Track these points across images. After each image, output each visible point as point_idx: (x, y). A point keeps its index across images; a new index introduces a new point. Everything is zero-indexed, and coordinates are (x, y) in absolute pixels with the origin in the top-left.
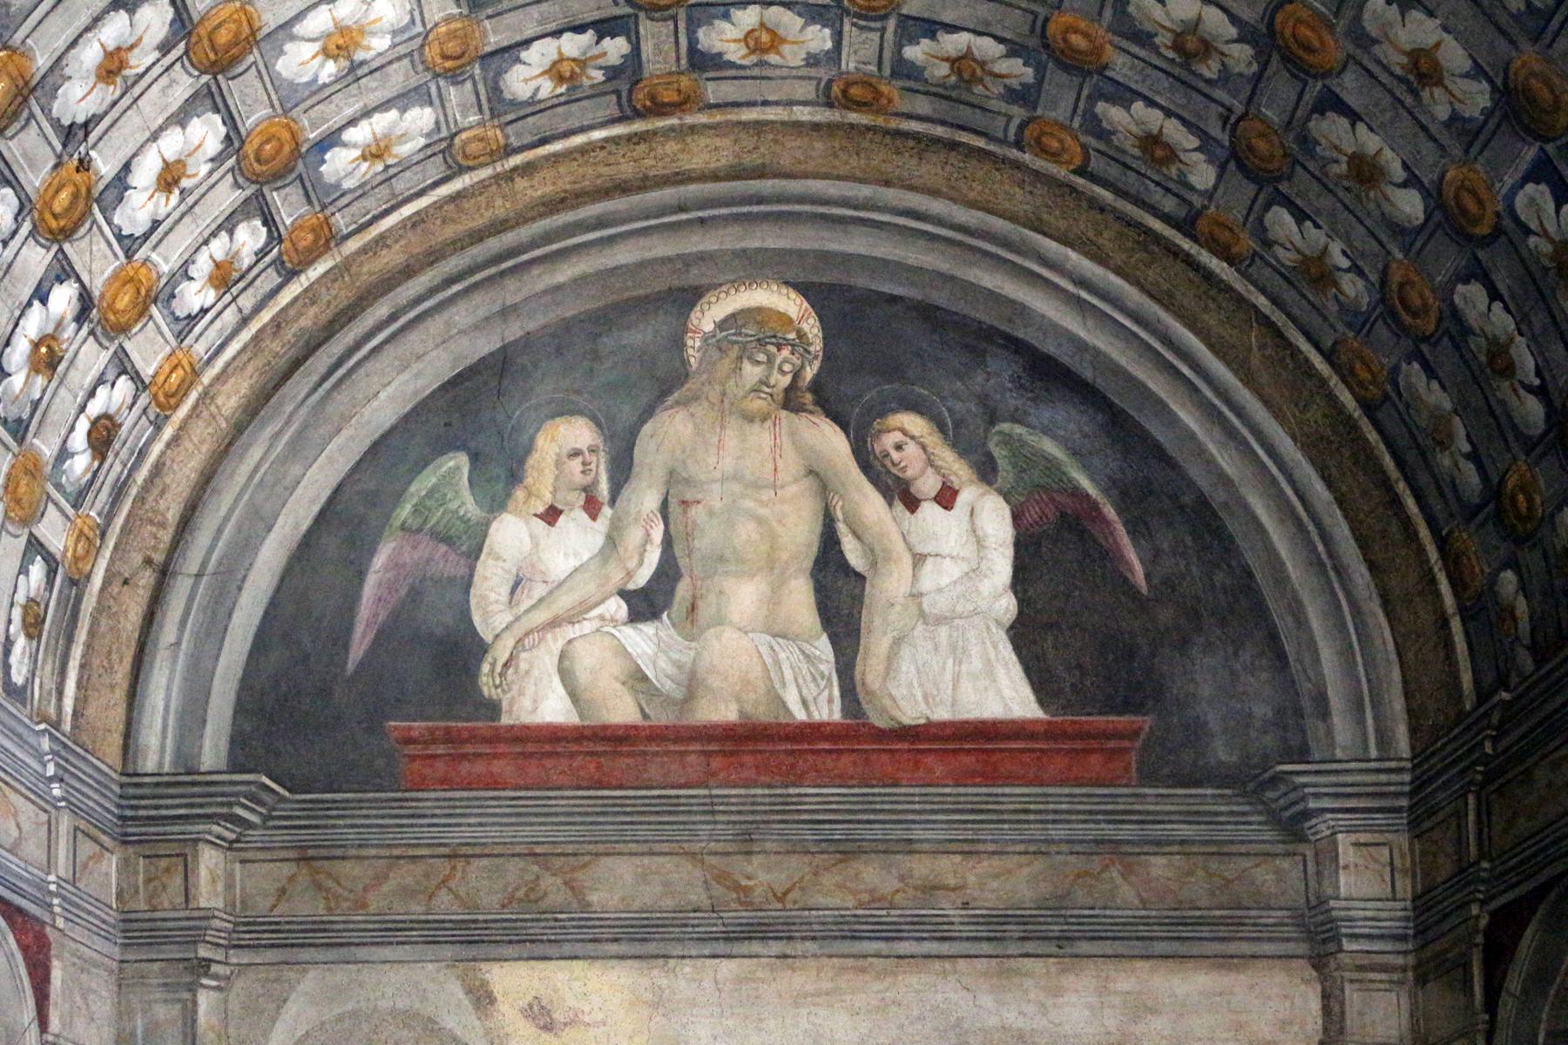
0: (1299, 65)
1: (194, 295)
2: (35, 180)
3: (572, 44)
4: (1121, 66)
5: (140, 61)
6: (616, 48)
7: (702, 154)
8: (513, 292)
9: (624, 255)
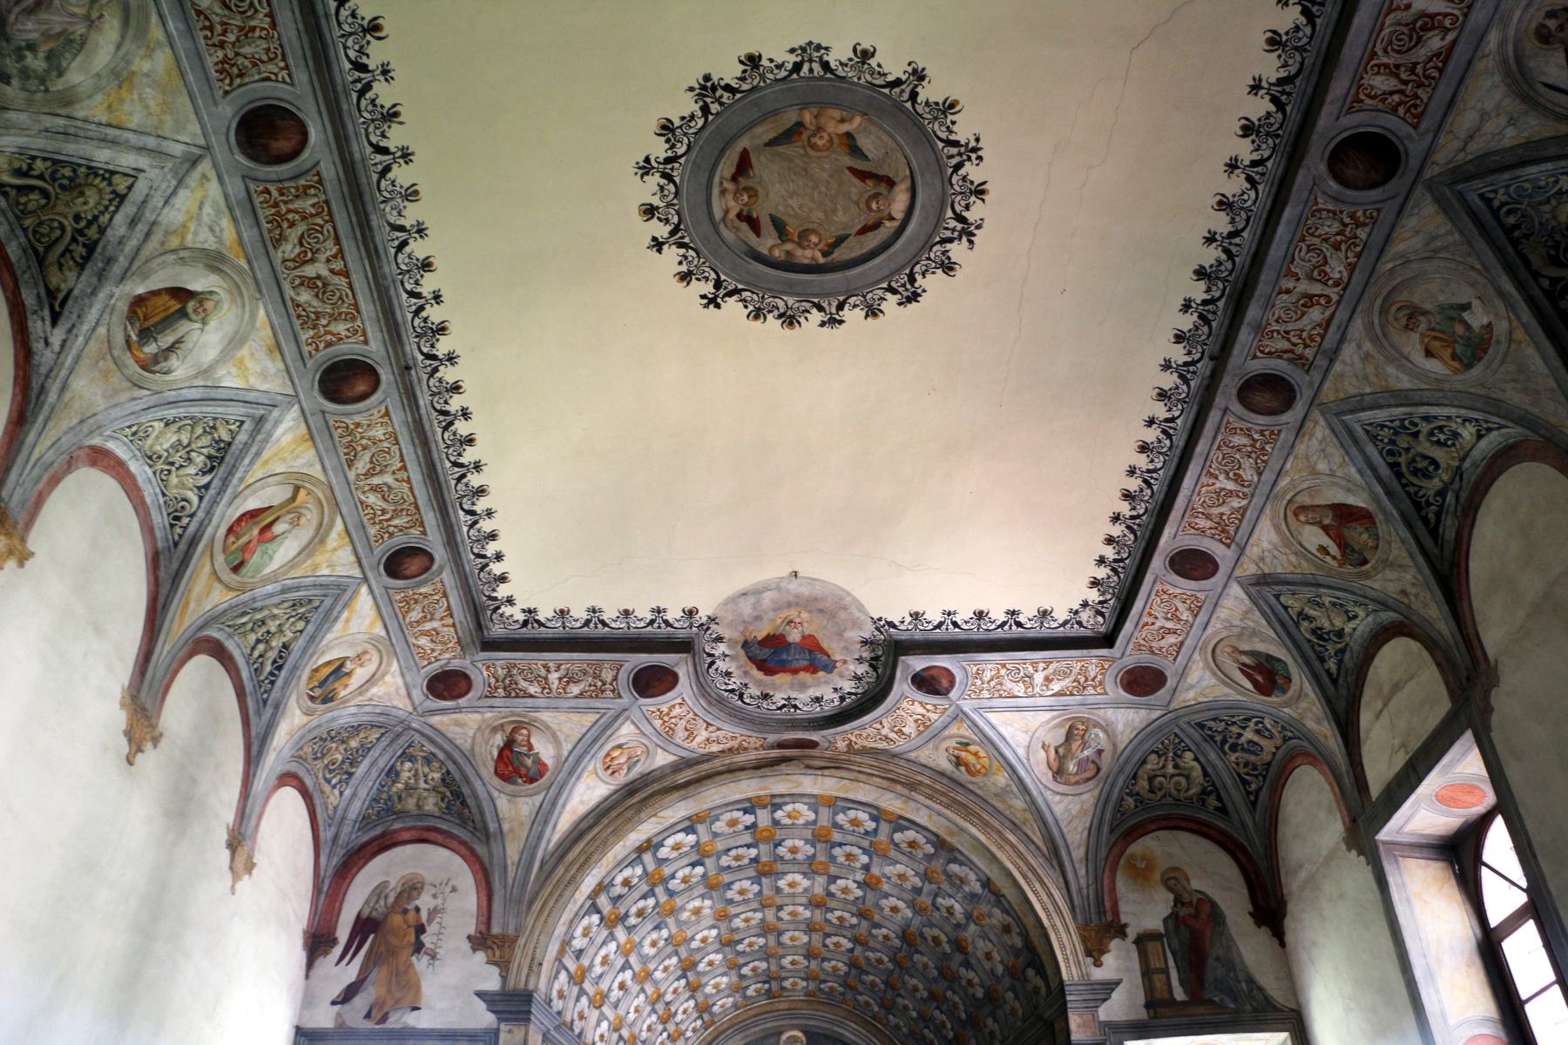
1: (689, 1034)
2: (661, 1012)
3: (759, 985)
4: (860, 988)
5: (680, 990)
6: (767, 986)
7: (782, 1006)
8: (748, 1032)
9: (768, 1025)
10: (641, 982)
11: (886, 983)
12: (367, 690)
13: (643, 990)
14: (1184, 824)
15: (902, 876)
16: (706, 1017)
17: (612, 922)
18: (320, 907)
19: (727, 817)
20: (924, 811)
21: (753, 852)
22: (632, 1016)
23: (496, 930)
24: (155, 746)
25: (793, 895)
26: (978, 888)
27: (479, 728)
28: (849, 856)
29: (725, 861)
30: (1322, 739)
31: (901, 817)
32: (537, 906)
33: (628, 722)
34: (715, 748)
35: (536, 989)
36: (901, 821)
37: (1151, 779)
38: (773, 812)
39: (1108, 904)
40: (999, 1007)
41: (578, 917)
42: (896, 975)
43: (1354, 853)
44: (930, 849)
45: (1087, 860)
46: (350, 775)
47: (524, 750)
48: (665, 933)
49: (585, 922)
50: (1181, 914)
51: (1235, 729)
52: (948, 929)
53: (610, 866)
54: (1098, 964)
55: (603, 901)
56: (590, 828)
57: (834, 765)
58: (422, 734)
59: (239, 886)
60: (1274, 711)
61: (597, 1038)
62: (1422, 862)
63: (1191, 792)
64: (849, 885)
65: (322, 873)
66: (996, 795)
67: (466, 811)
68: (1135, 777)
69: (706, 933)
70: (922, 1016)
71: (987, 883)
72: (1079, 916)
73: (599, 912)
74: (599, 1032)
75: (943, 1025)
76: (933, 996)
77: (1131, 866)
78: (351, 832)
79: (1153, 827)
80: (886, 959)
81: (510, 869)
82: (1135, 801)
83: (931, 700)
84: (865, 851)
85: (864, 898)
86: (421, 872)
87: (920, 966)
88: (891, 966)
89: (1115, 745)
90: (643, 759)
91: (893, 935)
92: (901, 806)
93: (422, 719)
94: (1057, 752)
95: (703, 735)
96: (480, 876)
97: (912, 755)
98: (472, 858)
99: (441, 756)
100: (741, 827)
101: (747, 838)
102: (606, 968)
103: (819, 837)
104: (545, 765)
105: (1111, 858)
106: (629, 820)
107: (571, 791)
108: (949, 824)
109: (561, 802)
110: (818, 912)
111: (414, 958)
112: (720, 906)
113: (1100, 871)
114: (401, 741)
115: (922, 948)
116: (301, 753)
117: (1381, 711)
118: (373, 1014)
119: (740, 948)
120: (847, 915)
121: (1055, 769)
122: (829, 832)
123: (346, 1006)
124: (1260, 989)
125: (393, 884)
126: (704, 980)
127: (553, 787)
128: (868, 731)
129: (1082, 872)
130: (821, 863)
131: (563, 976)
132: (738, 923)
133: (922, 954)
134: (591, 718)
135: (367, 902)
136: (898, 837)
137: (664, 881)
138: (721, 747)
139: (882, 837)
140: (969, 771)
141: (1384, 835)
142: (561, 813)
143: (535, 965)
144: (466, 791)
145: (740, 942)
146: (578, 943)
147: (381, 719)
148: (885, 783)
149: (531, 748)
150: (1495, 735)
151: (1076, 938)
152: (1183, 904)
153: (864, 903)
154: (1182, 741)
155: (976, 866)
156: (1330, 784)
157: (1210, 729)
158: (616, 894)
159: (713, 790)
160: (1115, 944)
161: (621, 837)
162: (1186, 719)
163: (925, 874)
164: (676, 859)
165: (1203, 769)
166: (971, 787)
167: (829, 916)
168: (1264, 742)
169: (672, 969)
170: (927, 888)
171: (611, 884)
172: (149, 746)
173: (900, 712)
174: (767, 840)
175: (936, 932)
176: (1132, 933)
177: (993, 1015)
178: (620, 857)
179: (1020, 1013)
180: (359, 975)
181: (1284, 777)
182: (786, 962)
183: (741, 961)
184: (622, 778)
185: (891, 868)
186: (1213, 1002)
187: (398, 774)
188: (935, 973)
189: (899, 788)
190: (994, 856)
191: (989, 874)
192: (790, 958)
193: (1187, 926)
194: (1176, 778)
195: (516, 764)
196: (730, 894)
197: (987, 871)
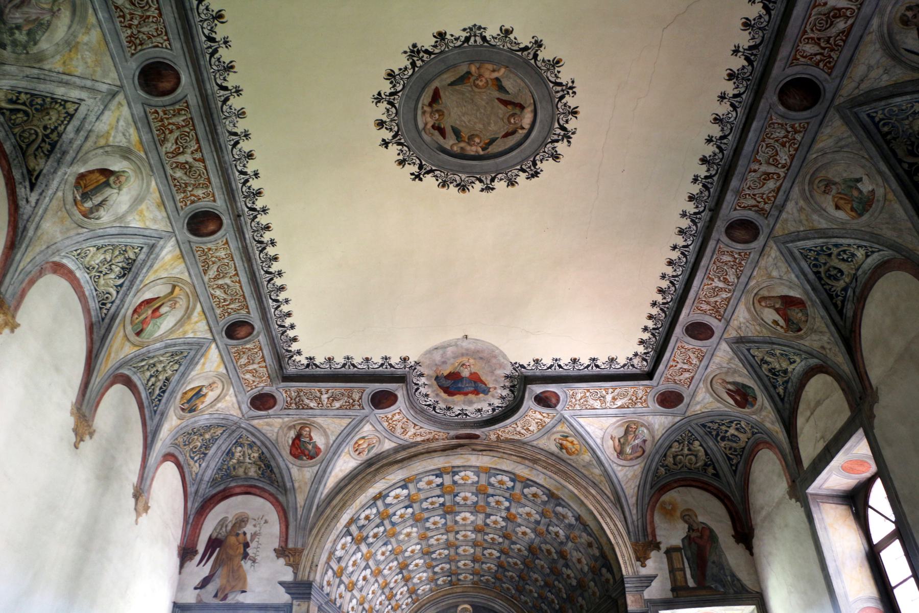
0: (523, 580)
1: (404, 606)
2: (387, 594)
3: (445, 578)
4: (504, 580)
5: (399, 581)
6: (449, 578)
7: (458, 590)
8: (438, 606)
9: (450, 601)
10: (376, 576)
11: (519, 577)
12: (215, 405)
13: (377, 581)
14: (694, 484)
15: (528, 514)
16: (414, 596)
17: (359, 541)
18: (187, 532)
19: (426, 479)
20: (542, 476)
21: (441, 500)
22: (370, 596)
23: (291, 545)
24: (91, 438)
25: (465, 525)
26: (573, 521)
27: (281, 427)
28: (498, 502)
29: (425, 505)
30: (775, 434)
31: (528, 479)
32: (315, 532)
33: (368, 424)
34: (419, 439)
35: (314, 580)
36: (528, 482)
37: (674, 457)
38: (453, 476)
39: (649, 530)
40: (586, 591)
41: (339, 538)
42: (525, 572)
43: (793, 500)
44: (545, 498)
45: (637, 504)
46: (205, 454)
47: (307, 440)
48: (390, 547)
49: (343, 541)
50: (692, 536)
51: (724, 428)
52: (556, 545)
53: (358, 508)
54: (643, 565)
55: (353, 529)
56: (346, 485)
57: (489, 449)
58: (247, 431)
59: (140, 519)
60: (747, 417)
61: (350, 609)
62: (834, 506)
63: (698, 465)
64: (498, 519)
65: (189, 512)
66: (584, 466)
67: (273, 476)
68: (665, 456)
69: (413, 547)
70: (540, 596)
71: (578, 518)
72: (632, 537)
73: (351, 535)
74: (351, 605)
75: (553, 601)
76: (547, 584)
77: (663, 508)
78: (206, 488)
79: (676, 485)
80: (519, 562)
81: (299, 510)
82: (666, 470)
83: (546, 410)
84: (507, 499)
85: (506, 527)
86: (246, 511)
87: (539, 567)
88: (522, 567)
89: (653, 437)
90: (377, 445)
91: (523, 549)
92: (528, 473)
93: (248, 422)
94: (619, 441)
95: (412, 431)
96: (281, 514)
97: (535, 443)
98: (277, 503)
99: (259, 443)
100: (434, 485)
101: (438, 492)
102: (355, 568)
103: (480, 491)
104: (319, 449)
105: (651, 503)
106: (369, 481)
107: (335, 464)
108: (556, 483)
109: (329, 470)
110: (479, 535)
111: (242, 562)
112: (422, 532)
113: (645, 511)
114: (235, 435)
115: (540, 556)
116: (176, 442)
117: (809, 417)
118: (219, 595)
119: (434, 556)
120: (496, 537)
121: (618, 451)
122: (486, 488)
123: (203, 590)
124: (739, 580)
125: (230, 518)
126: (412, 575)
127: (324, 462)
128: (509, 429)
129: (634, 512)
130: (481, 506)
131: (330, 573)
132: (432, 541)
133: (540, 560)
134: (346, 421)
135: (215, 529)
136: (526, 491)
137: (389, 517)
138: (422, 438)
139: (517, 491)
140: (568, 452)
141: (811, 490)
142: (329, 477)
143: (314, 566)
144: (273, 464)
145: (434, 552)
146: (339, 553)
147: (223, 422)
148: (519, 460)
149: (311, 439)
150: (876, 431)
151: (630, 550)
152: (693, 530)
153: (506, 529)
154: (693, 435)
155: (572, 508)
156: (779, 460)
157: (709, 427)
158: (361, 524)
159: (418, 464)
160: (653, 554)
161: (364, 491)
162: (695, 422)
163: (542, 513)
164: (396, 504)
165: (705, 451)
166: (569, 462)
167: (486, 537)
168: (741, 435)
169: (394, 568)
170: (543, 521)
171: (358, 519)
172: (87, 437)
173: (528, 418)
174: (449, 493)
175: (549, 547)
176: (663, 547)
177: (582, 595)
178: (363, 503)
179: (598, 594)
180: (210, 572)
181: (752, 456)
182: (461, 564)
183: (434, 564)
184: (365, 457)
185: (522, 509)
186: (711, 588)
187: (233, 454)
188: (548, 571)
189: (527, 462)
190: (582, 502)
191: (580, 513)
192: (463, 562)
193: (696, 543)
194: (689, 457)
195: (303, 448)
196: (428, 525)
197: (579, 511)
